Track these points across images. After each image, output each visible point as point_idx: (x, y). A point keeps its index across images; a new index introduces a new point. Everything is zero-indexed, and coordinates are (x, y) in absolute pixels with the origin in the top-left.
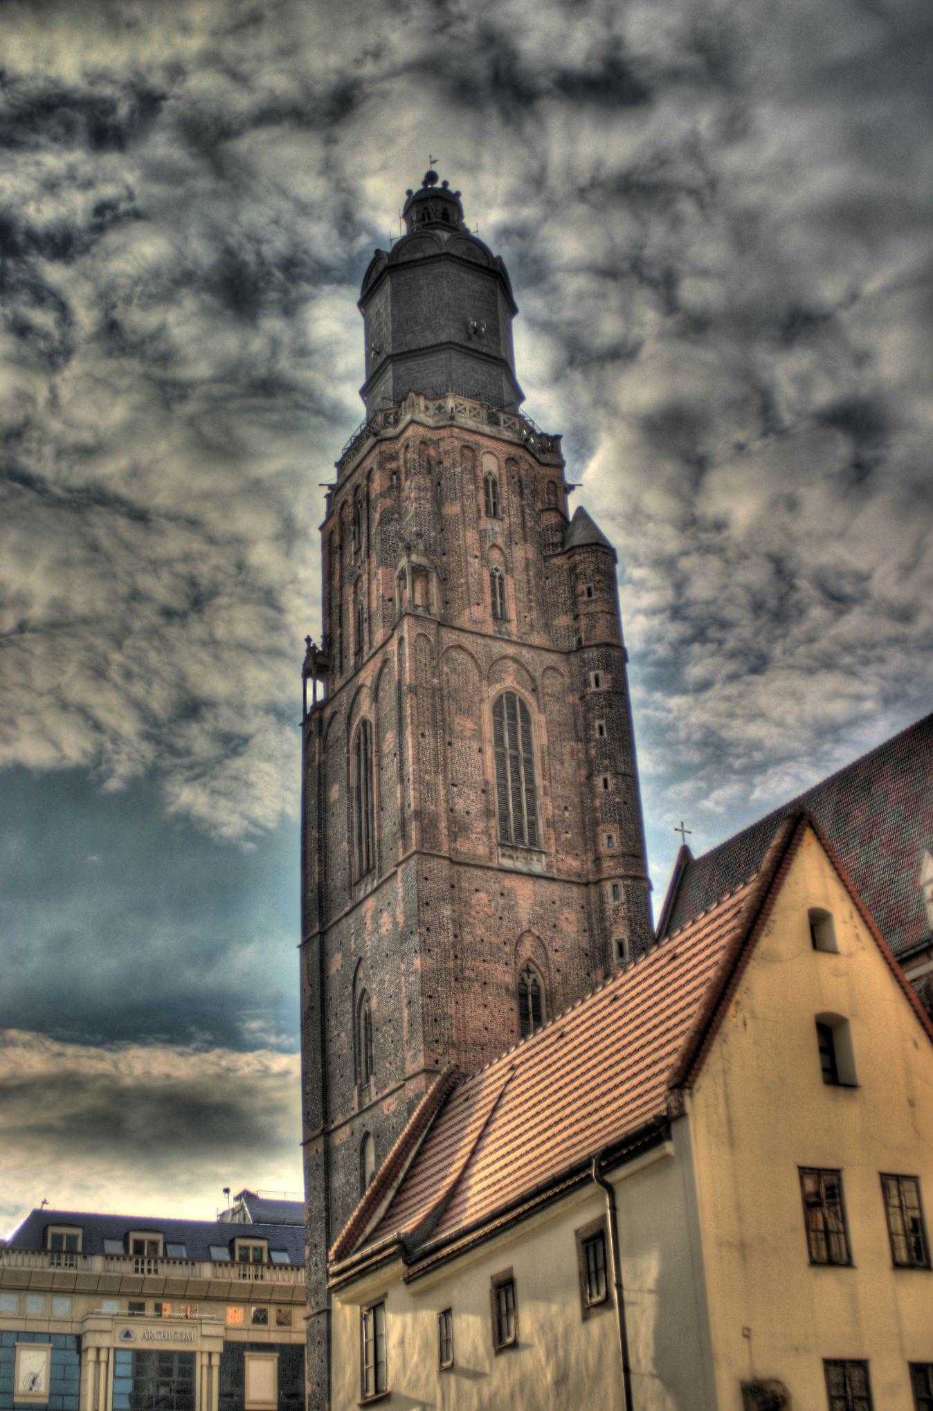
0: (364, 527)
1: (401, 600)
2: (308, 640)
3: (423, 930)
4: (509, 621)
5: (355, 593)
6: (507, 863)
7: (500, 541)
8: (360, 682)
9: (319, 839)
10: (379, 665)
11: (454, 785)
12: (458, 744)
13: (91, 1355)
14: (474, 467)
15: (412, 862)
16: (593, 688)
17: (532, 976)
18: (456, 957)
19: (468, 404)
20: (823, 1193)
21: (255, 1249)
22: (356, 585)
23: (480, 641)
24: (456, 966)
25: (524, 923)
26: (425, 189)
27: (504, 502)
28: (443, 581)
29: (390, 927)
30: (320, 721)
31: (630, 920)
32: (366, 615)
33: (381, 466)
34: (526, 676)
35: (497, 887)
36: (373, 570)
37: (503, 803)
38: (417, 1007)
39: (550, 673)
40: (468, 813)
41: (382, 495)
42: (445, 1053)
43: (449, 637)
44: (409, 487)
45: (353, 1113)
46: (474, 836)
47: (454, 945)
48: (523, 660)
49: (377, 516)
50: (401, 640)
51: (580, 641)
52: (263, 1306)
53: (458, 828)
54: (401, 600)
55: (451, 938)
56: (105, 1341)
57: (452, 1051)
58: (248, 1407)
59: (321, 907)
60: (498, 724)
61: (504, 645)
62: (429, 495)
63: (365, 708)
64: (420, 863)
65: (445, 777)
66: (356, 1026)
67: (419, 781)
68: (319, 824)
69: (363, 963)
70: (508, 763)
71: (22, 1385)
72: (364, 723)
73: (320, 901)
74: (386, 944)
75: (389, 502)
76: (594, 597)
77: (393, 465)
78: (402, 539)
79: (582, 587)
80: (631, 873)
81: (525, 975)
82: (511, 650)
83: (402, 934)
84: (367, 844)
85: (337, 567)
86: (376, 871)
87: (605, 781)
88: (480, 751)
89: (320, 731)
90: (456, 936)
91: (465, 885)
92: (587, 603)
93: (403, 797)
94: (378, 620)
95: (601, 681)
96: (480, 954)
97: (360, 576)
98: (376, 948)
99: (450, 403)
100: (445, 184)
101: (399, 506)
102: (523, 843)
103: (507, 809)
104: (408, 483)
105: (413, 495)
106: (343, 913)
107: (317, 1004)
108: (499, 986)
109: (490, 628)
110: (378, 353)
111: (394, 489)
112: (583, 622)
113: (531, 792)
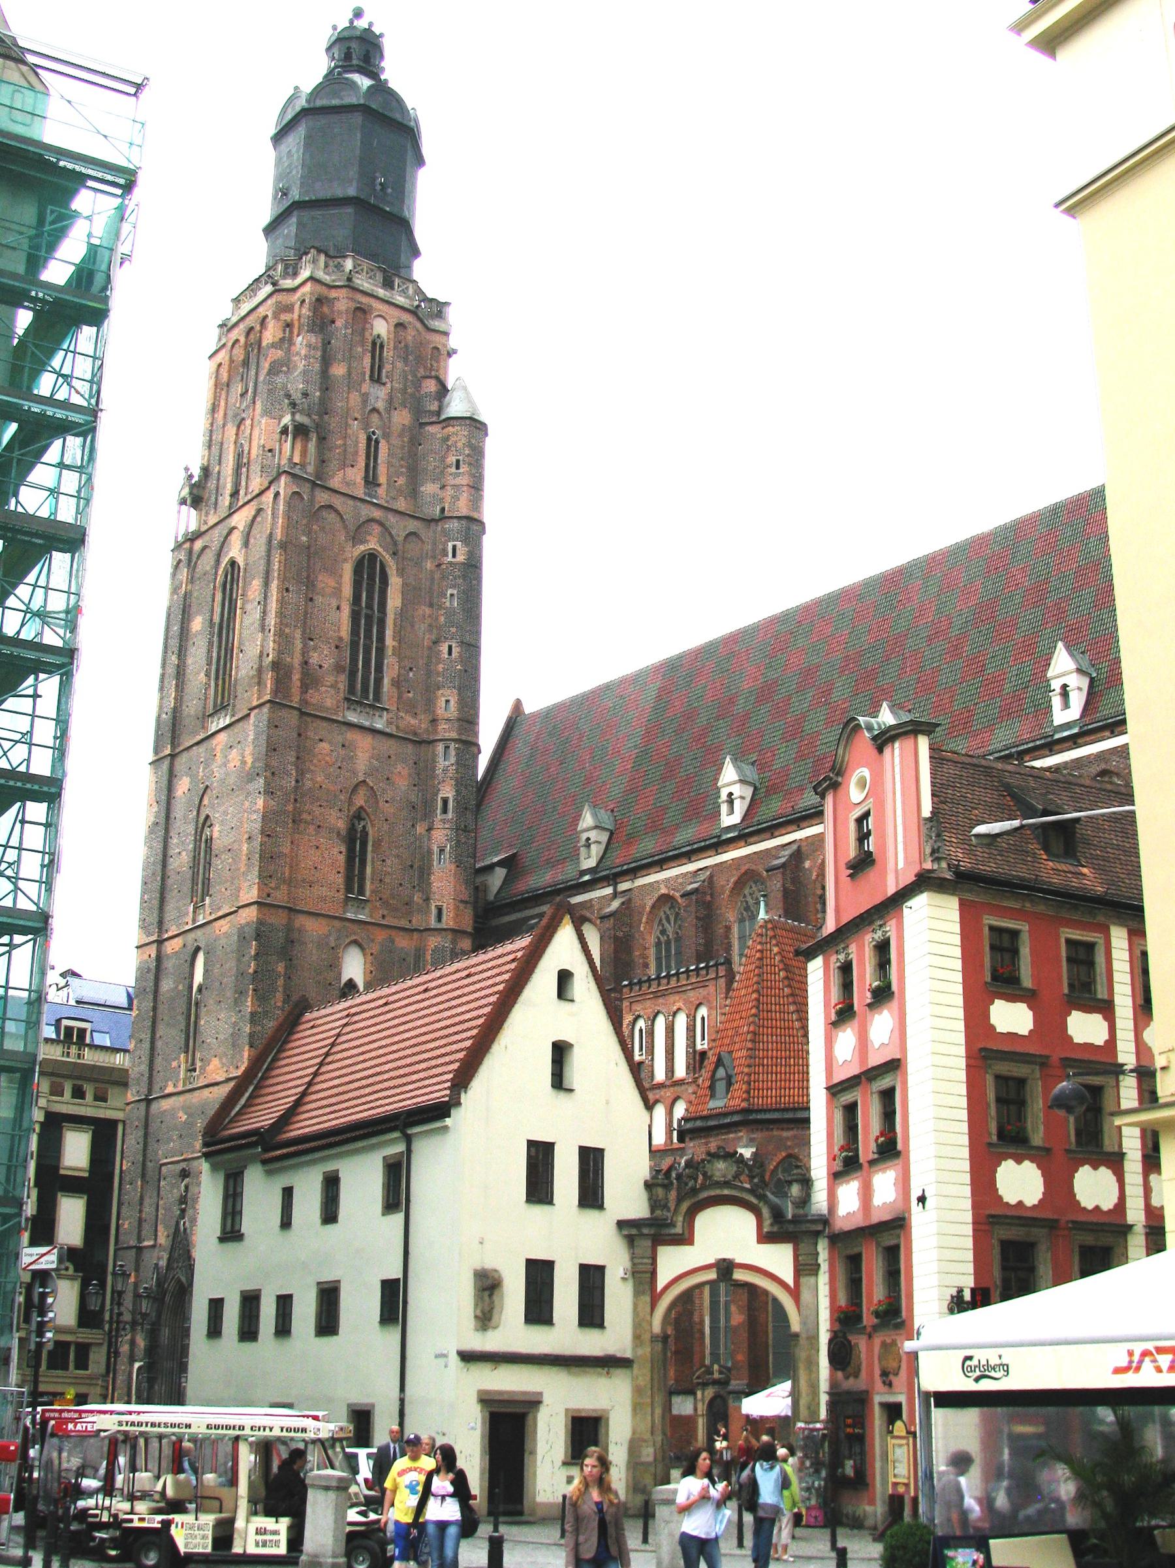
0: (253, 372)
1: (280, 453)
2: (187, 469)
3: (268, 774)
4: (379, 485)
5: (237, 434)
6: (352, 717)
7: (380, 405)
8: (233, 524)
9: (178, 666)
10: (253, 513)
11: (312, 640)
12: (319, 599)
14: (364, 329)
15: (265, 709)
16: (450, 558)
17: (362, 823)
18: (296, 800)
19: (366, 264)
20: (540, 1157)
21: (79, 1029)
22: (238, 427)
23: (351, 502)
24: (295, 809)
26: (351, 26)
27: (387, 368)
28: (322, 439)
29: (238, 764)
30: (191, 551)
32: (245, 460)
33: (276, 316)
34: (388, 539)
35: (340, 739)
36: (257, 417)
37: (354, 660)
38: (257, 843)
39: (413, 538)
40: (321, 667)
41: (273, 345)
42: (277, 888)
43: (323, 497)
44: (300, 342)
45: (187, 928)
46: (323, 689)
47: (296, 788)
48: (388, 524)
49: (267, 365)
50: (277, 494)
51: (443, 510)
52: (80, 1082)
53: (310, 680)
54: (280, 453)
57: (284, 887)
59: (174, 731)
60: (357, 585)
61: (373, 508)
62: (319, 354)
63: (235, 551)
64: (271, 711)
65: (304, 632)
66: (197, 849)
67: (280, 633)
68: (180, 651)
69: (209, 791)
70: (363, 622)
72: (233, 563)
73: (174, 725)
74: (232, 780)
75: (279, 354)
76: (461, 470)
77: (286, 317)
78: (288, 396)
79: (452, 459)
80: (464, 738)
82: (377, 514)
83: (248, 774)
84: (224, 680)
85: (222, 403)
86: (230, 708)
87: (450, 647)
88: (338, 608)
89: (190, 561)
90: (297, 781)
91: (310, 734)
92: (456, 475)
93: (262, 646)
94: (255, 468)
95: (458, 552)
97: (243, 419)
98: (223, 781)
99: (349, 264)
100: (371, 24)
101: (289, 360)
102: (367, 699)
103: (357, 665)
104: (300, 338)
105: (303, 352)
106: (195, 741)
107: (162, 821)
108: (331, 831)
109: (360, 492)
110: (284, 194)
111: (285, 342)
112: (449, 491)
113: (381, 650)
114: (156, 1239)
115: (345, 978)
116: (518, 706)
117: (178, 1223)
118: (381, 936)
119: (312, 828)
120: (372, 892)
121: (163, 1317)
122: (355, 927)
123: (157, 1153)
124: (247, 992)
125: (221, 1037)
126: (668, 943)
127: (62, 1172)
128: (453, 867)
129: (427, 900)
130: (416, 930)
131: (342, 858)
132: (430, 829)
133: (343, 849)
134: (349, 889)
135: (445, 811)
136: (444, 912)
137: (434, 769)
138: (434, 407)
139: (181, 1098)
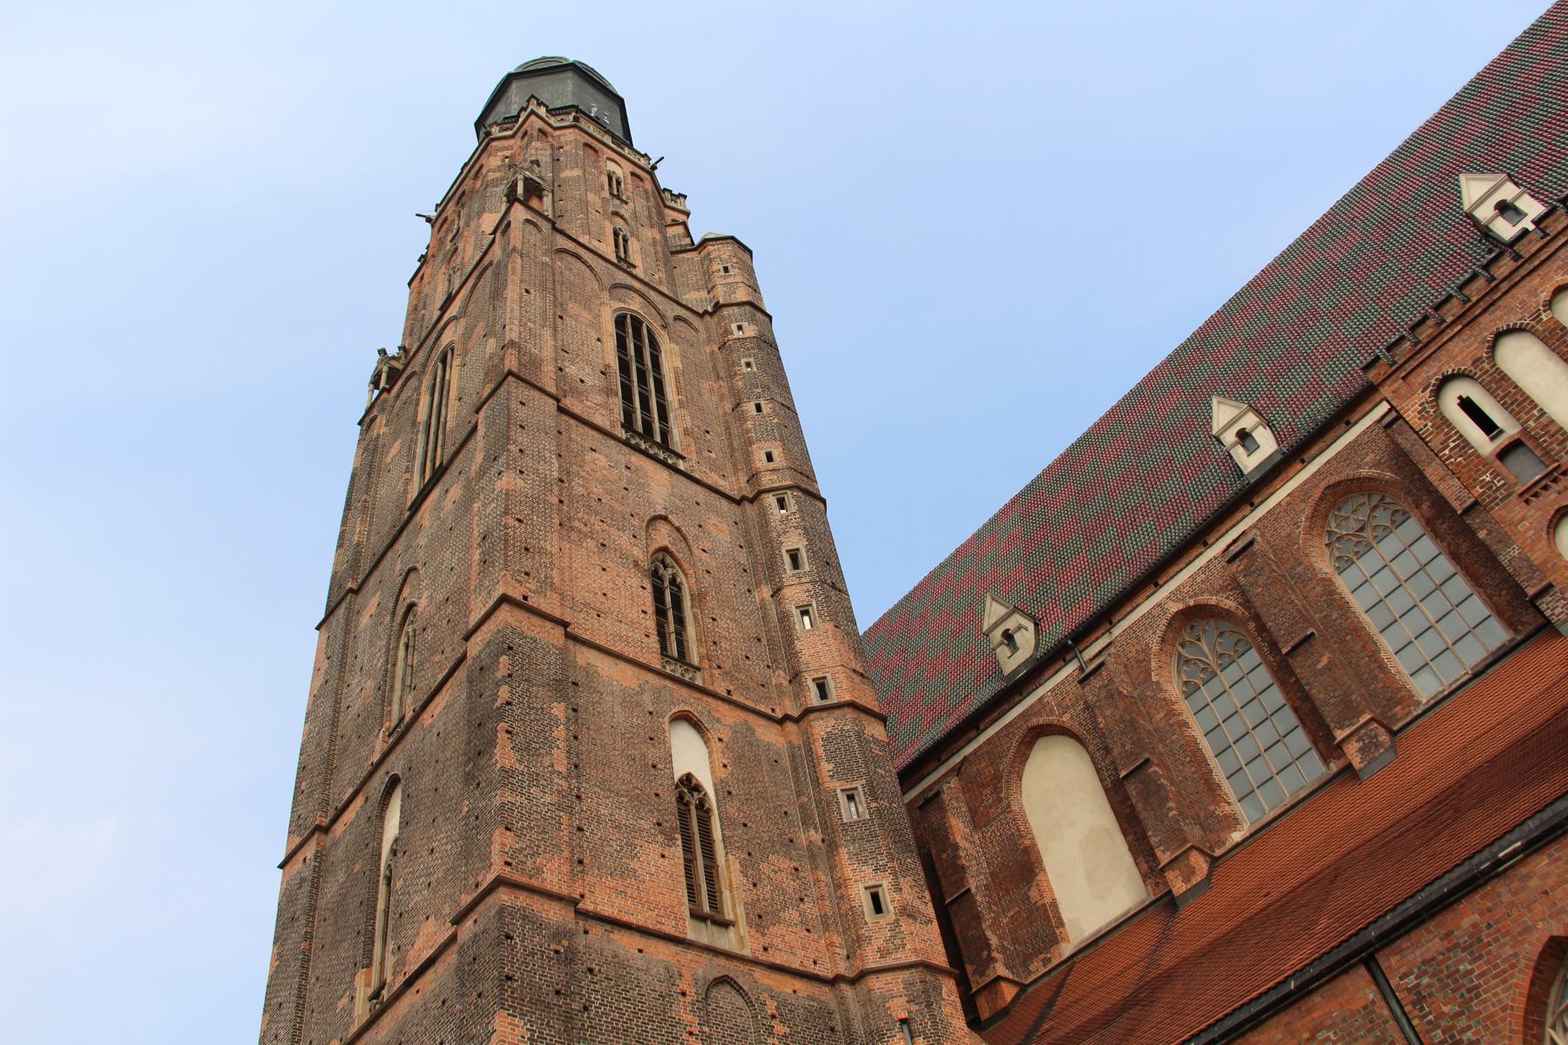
17: (670, 571)
115: (678, 773)
118: (731, 716)
119: (591, 543)
120: (701, 658)
128: (830, 626)
129: (796, 677)
132: (776, 592)
138: (688, 241)
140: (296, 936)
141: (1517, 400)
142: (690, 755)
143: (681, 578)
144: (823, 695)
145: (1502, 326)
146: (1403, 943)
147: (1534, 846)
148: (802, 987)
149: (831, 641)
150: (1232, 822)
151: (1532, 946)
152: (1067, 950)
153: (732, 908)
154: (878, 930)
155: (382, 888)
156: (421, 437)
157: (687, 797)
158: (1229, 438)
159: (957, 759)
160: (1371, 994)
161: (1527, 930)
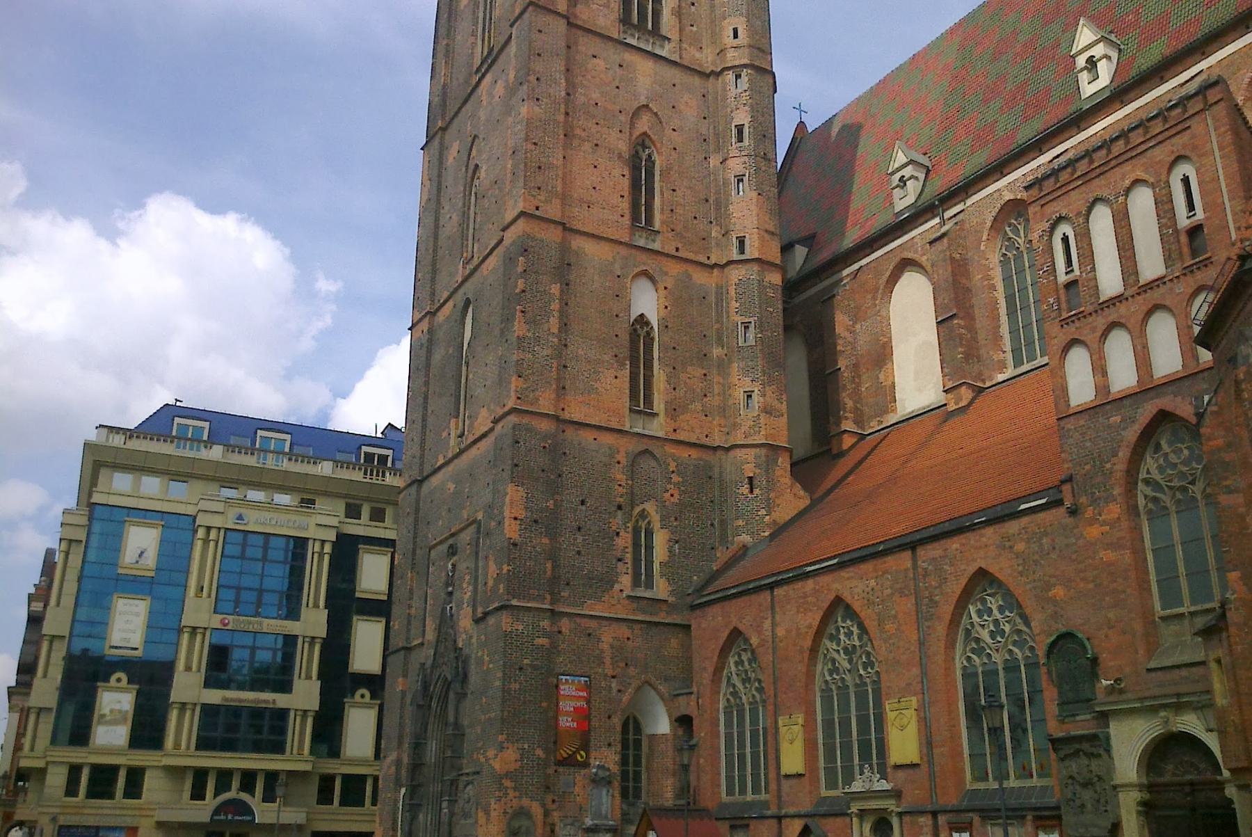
13: (201, 533)
17: (647, 152)
21: (379, 456)
25: (643, 98)
31: (752, 106)
55: (563, 94)
56: (217, 521)
58: (358, 595)
71: (129, 556)
81: (640, 148)
96: (594, 117)
114: (424, 636)
115: (634, 314)
116: (801, 125)
117: (444, 609)
118: (675, 269)
120: (663, 222)
121: (430, 727)
122: (643, 257)
123: (427, 538)
124: (514, 315)
125: (489, 383)
126: (1019, 257)
127: (358, 595)
128: (754, 194)
130: (716, 265)
131: (626, 182)
133: (626, 172)
134: (635, 218)
135: (740, 139)
136: (747, 242)
137: (725, 99)
139: (450, 468)
140: (421, 381)
141: (1088, 256)
142: (646, 302)
143: (655, 156)
144: (742, 251)
145: (1099, 193)
146: (929, 547)
147: (989, 523)
148: (694, 453)
149: (753, 207)
150: (1002, 366)
151: (972, 569)
152: (892, 419)
153: (659, 405)
154: (748, 415)
155: (464, 368)
156: (480, 42)
157: (640, 331)
158: (1081, 61)
159: (856, 266)
160: (909, 564)
161: (974, 560)
